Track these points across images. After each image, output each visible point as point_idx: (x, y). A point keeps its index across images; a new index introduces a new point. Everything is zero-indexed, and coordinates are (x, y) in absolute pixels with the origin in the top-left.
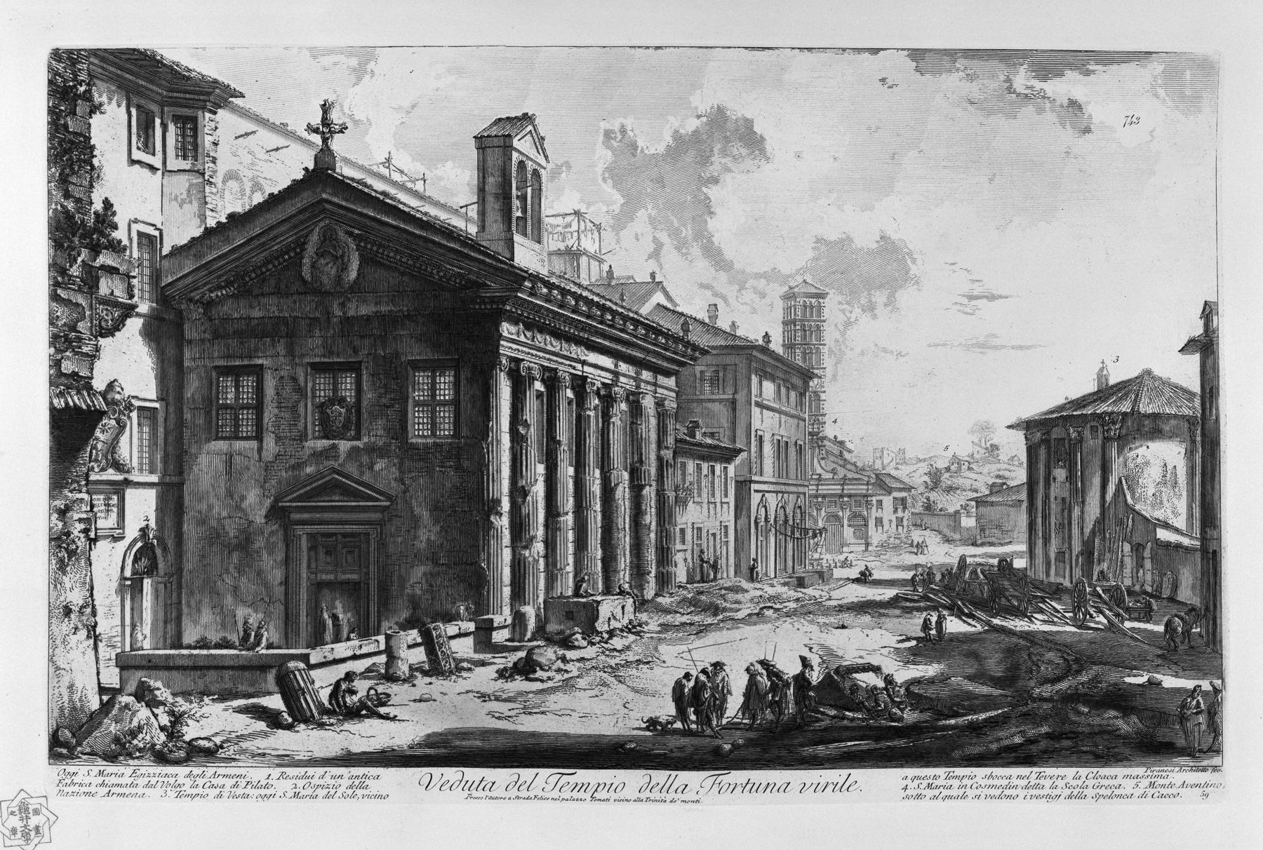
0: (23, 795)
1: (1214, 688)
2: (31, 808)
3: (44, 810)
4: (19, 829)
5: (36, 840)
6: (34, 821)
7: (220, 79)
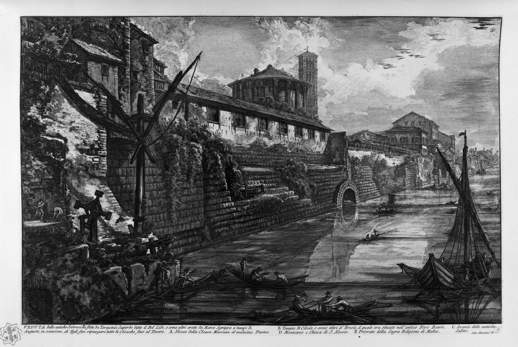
0: (8, 325)
1: (149, 103)
2: (12, 329)
3: (17, 329)
4: (9, 337)
5: (16, 340)
6: (13, 333)
7: (318, 72)
